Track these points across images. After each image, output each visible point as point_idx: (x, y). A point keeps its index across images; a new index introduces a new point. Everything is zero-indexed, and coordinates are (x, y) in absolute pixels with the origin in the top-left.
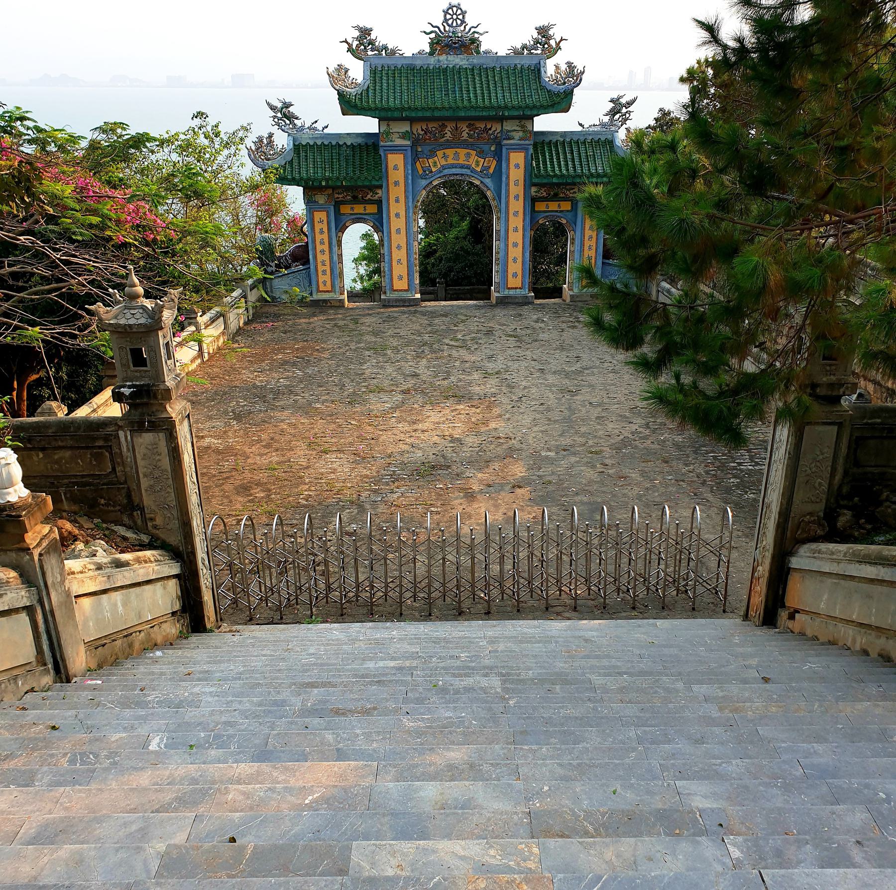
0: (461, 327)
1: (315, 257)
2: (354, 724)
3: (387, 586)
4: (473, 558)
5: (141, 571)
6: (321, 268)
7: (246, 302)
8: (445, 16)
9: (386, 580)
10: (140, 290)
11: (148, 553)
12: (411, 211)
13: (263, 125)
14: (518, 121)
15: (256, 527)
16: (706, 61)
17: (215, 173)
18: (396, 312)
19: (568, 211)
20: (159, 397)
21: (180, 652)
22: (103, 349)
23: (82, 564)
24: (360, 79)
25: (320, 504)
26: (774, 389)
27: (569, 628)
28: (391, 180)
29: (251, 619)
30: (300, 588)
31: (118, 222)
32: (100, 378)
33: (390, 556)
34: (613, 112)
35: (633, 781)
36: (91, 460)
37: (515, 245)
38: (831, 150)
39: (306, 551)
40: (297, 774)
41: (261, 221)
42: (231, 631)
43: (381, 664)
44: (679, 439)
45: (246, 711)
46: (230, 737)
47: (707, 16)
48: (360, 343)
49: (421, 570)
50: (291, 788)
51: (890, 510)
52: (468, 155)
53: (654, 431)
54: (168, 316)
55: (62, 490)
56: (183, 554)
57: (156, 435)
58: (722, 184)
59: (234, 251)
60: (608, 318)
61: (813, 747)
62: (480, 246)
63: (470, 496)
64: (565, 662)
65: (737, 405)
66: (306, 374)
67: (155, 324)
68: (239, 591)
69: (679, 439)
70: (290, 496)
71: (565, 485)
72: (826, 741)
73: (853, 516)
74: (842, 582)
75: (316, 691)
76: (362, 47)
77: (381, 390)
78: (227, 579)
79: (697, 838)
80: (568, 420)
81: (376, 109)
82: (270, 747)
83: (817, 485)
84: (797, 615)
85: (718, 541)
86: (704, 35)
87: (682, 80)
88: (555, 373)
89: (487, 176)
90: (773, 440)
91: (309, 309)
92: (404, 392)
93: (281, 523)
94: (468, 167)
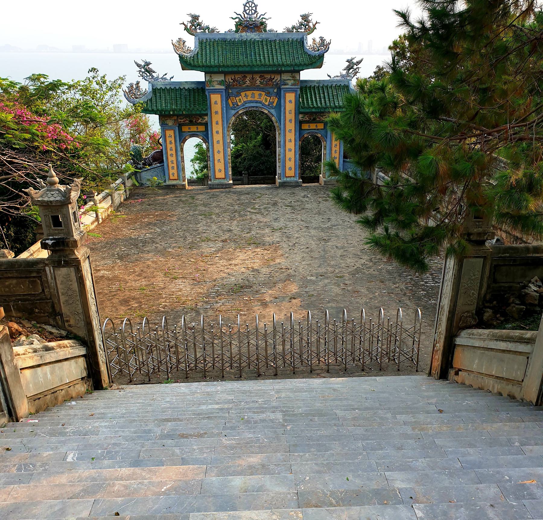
0: (258, 201)
1: (167, 158)
2: (193, 443)
3: (214, 360)
4: (266, 342)
5: (62, 353)
6: (171, 165)
7: (125, 187)
8: (244, 8)
9: (213, 356)
10: (56, 179)
11: (66, 342)
12: (226, 129)
13: (133, 76)
14: (290, 74)
15: (133, 325)
16: (405, 36)
17: (104, 107)
18: (217, 192)
19: (322, 129)
20: (70, 245)
21: (87, 402)
22: (35, 216)
23: (24, 349)
24: (193, 48)
25: (172, 310)
26: (445, 237)
27: (324, 383)
28: (213, 111)
29: (131, 382)
30: (161, 362)
31: (43, 137)
32: (35, 235)
33: (216, 341)
34: (348, 68)
35: (360, 472)
36: (29, 285)
37: (290, 150)
38: (476, 90)
39: (163, 340)
40: (157, 473)
41: (133, 136)
42: (118, 389)
43: (210, 407)
44: (390, 268)
45: (127, 436)
46: (116, 452)
47: (402, 8)
48: (195, 211)
49: (235, 350)
50: (153, 482)
51: (514, 309)
52: (260, 95)
53: (375, 263)
54: (74, 195)
55: (11, 304)
56: (87, 342)
57: (68, 269)
58: (413, 111)
59: (117, 155)
60: (345, 194)
61: (467, 450)
62: (268, 151)
63: (265, 304)
64: (321, 403)
65: (423, 246)
66: (162, 230)
67: (66, 201)
68: (123, 364)
69: (390, 268)
70: (154, 306)
71: (322, 297)
72: (475, 446)
73: (493, 313)
74: (486, 352)
75: (170, 424)
76: (194, 27)
77: (209, 240)
78: (115, 357)
79: (398, 506)
80: (323, 257)
81: (203, 66)
82: (141, 458)
83: (471, 294)
84: (460, 372)
85: (413, 329)
86: (400, 20)
87: (390, 48)
88: (315, 228)
89: (272, 108)
90: (444, 268)
91: (163, 191)
92: (223, 241)
93: (148, 322)
94: (260, 102)
